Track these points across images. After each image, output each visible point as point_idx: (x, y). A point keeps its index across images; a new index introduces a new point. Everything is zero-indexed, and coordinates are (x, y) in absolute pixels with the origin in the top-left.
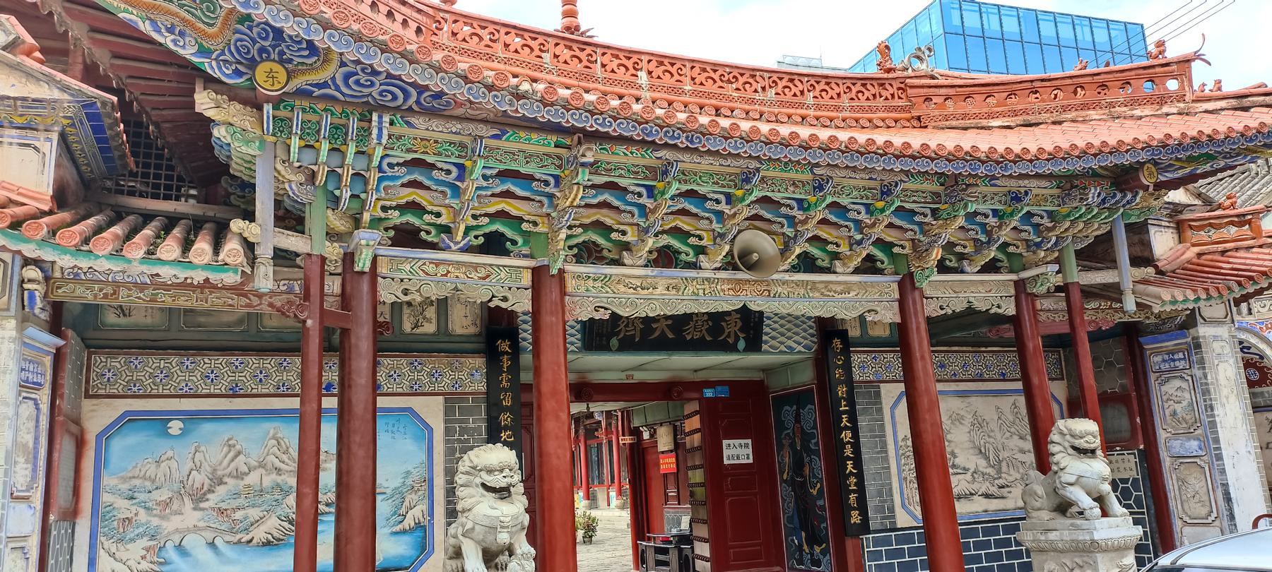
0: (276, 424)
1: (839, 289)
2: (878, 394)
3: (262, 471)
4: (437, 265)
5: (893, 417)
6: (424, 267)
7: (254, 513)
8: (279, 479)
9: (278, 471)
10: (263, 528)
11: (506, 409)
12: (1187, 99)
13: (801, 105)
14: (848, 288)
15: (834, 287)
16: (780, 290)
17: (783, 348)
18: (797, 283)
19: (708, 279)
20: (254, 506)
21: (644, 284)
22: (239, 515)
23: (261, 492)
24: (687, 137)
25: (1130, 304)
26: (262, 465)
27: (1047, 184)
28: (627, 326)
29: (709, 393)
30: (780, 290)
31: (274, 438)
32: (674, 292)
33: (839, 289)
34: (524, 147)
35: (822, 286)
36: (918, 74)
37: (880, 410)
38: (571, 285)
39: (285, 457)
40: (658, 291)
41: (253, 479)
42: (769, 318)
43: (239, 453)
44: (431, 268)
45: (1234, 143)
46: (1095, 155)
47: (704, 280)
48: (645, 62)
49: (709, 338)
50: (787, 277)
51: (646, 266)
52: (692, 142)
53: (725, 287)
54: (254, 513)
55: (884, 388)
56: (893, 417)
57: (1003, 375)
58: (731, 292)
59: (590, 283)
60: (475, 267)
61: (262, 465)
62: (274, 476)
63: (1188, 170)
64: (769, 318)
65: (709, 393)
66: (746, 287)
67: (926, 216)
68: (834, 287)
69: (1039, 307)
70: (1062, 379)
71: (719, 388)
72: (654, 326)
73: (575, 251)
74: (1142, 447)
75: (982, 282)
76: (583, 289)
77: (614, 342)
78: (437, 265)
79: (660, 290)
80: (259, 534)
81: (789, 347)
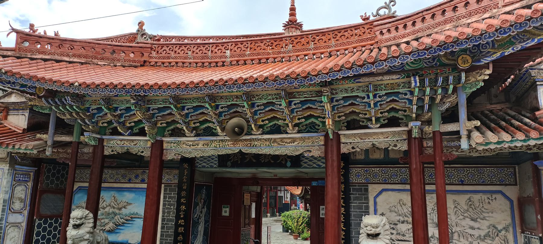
0: (114, 192)
1: (288, 141)
2: (367, 190)
3: (109, 207)
4: (121, 141)
5: (375, 203)
6: (117, 142)
7: (107, 221)
8: (114, 210)
9: (114, 208)
10: (108, 226)
11: (184, 190)
12: (500, 6)
13: (329, 47)
14: (294, 140)
15: (285, 140)
16: (256, 143)
17: (314, 165)
18: (266, 140)
19: (222, 140)
20: (107, 218)
21: (194, 144)
22: (103, 221)
23: (109, 214)
24: (143, 91)
25: (464, 144)
26: (110, 205)
27: (398, 76)
28: (234, 157)
29: (314, 184)
30: (256, 143)
31: (114, 197)
32: (206, 146)
33: (288, 141)
34: (125, 98)
35: (279, 140)
36: (382, 18)
37: (367, 199)
38: (165, 146)
39: (116, 203)
40: (199, 147)
41: (107, 210)
42: (198, 159)
43: (104, 201)
44: (119, 142)
45: (490, 37)
46: (373, 63)
47: (220, 140)
48: (230, 46)
49: (272, 162)
50: (260, 137)
51: (195, 136)
52: (146, 93)
53: (229, 143)
54: (107, 221)
55: (371, 187)
56: (375, 203)
57: (462, 181)
58: (232, 145)
59: (172, 144)
60: (133, 141)
61: (110, 205)
62: (112, 209)
63: (498, 54)
64: (198, 159)
65: (314, 184)
66: (239, 143)
67: (406, 94)
68: (285, 140)
69: (425, 145)
70: (516, 185)
71: (320, 181)
72: (246, 157)
73: (170, 132)
74: (541, 235)
75: (382, 133)
76: (169, 147)
77: (229, 163)
78: (121, 141)
79: (200, 146)
80: (107, 228)
81: (319, 165)
